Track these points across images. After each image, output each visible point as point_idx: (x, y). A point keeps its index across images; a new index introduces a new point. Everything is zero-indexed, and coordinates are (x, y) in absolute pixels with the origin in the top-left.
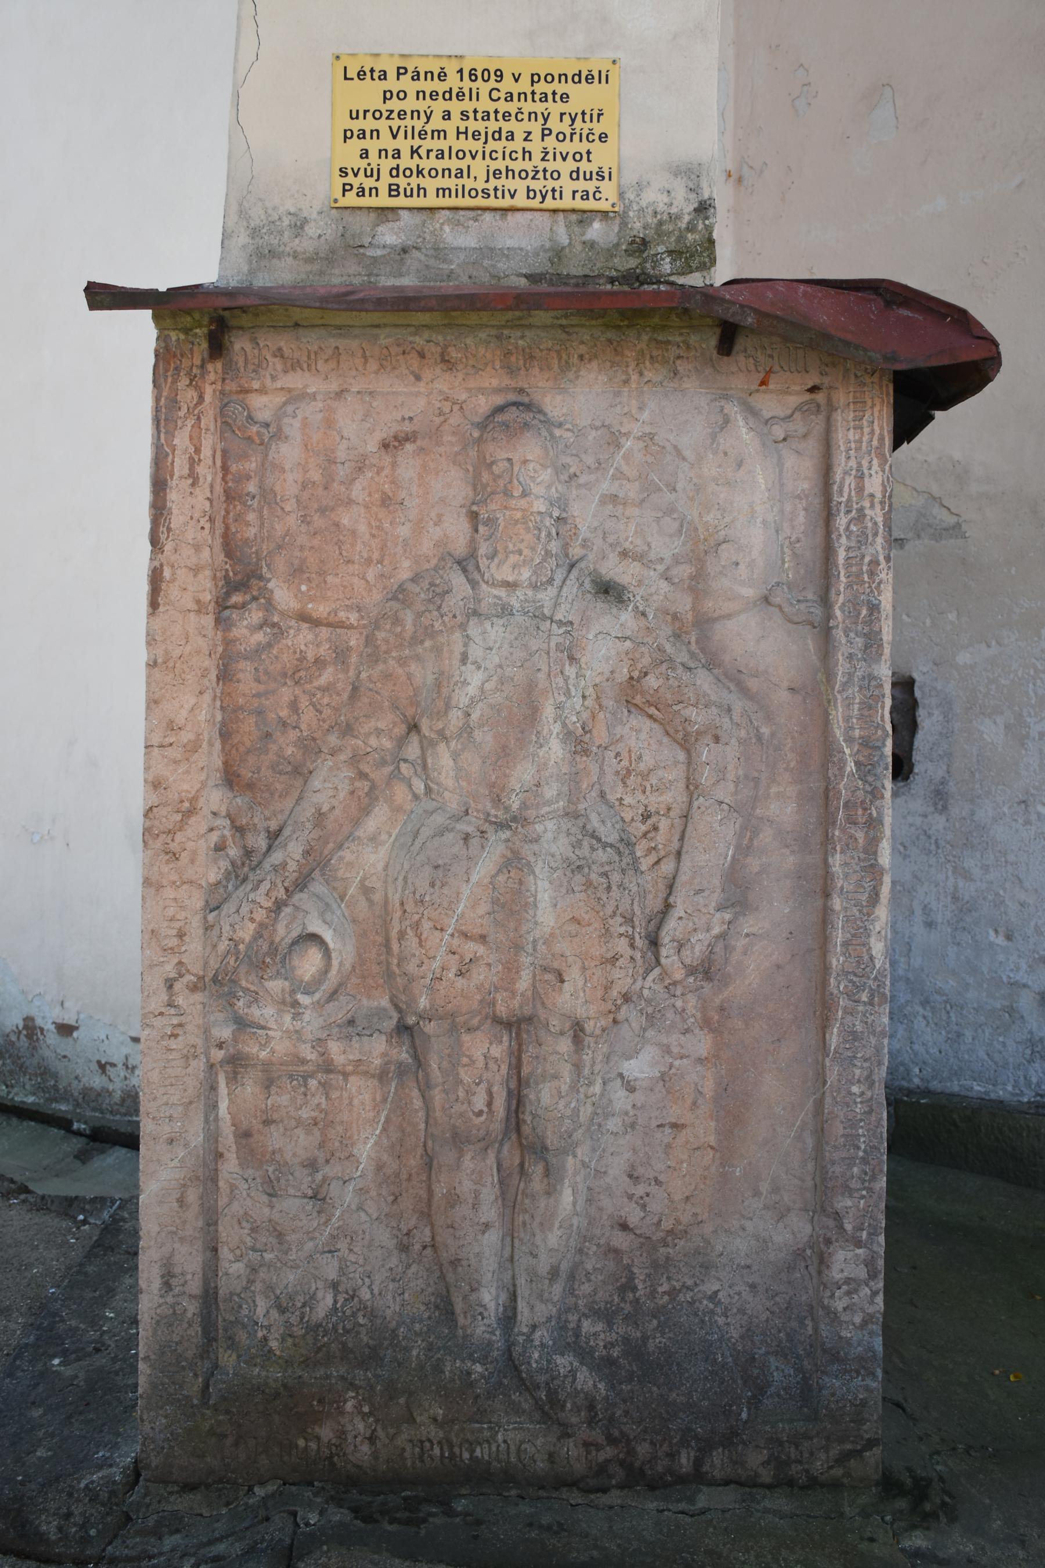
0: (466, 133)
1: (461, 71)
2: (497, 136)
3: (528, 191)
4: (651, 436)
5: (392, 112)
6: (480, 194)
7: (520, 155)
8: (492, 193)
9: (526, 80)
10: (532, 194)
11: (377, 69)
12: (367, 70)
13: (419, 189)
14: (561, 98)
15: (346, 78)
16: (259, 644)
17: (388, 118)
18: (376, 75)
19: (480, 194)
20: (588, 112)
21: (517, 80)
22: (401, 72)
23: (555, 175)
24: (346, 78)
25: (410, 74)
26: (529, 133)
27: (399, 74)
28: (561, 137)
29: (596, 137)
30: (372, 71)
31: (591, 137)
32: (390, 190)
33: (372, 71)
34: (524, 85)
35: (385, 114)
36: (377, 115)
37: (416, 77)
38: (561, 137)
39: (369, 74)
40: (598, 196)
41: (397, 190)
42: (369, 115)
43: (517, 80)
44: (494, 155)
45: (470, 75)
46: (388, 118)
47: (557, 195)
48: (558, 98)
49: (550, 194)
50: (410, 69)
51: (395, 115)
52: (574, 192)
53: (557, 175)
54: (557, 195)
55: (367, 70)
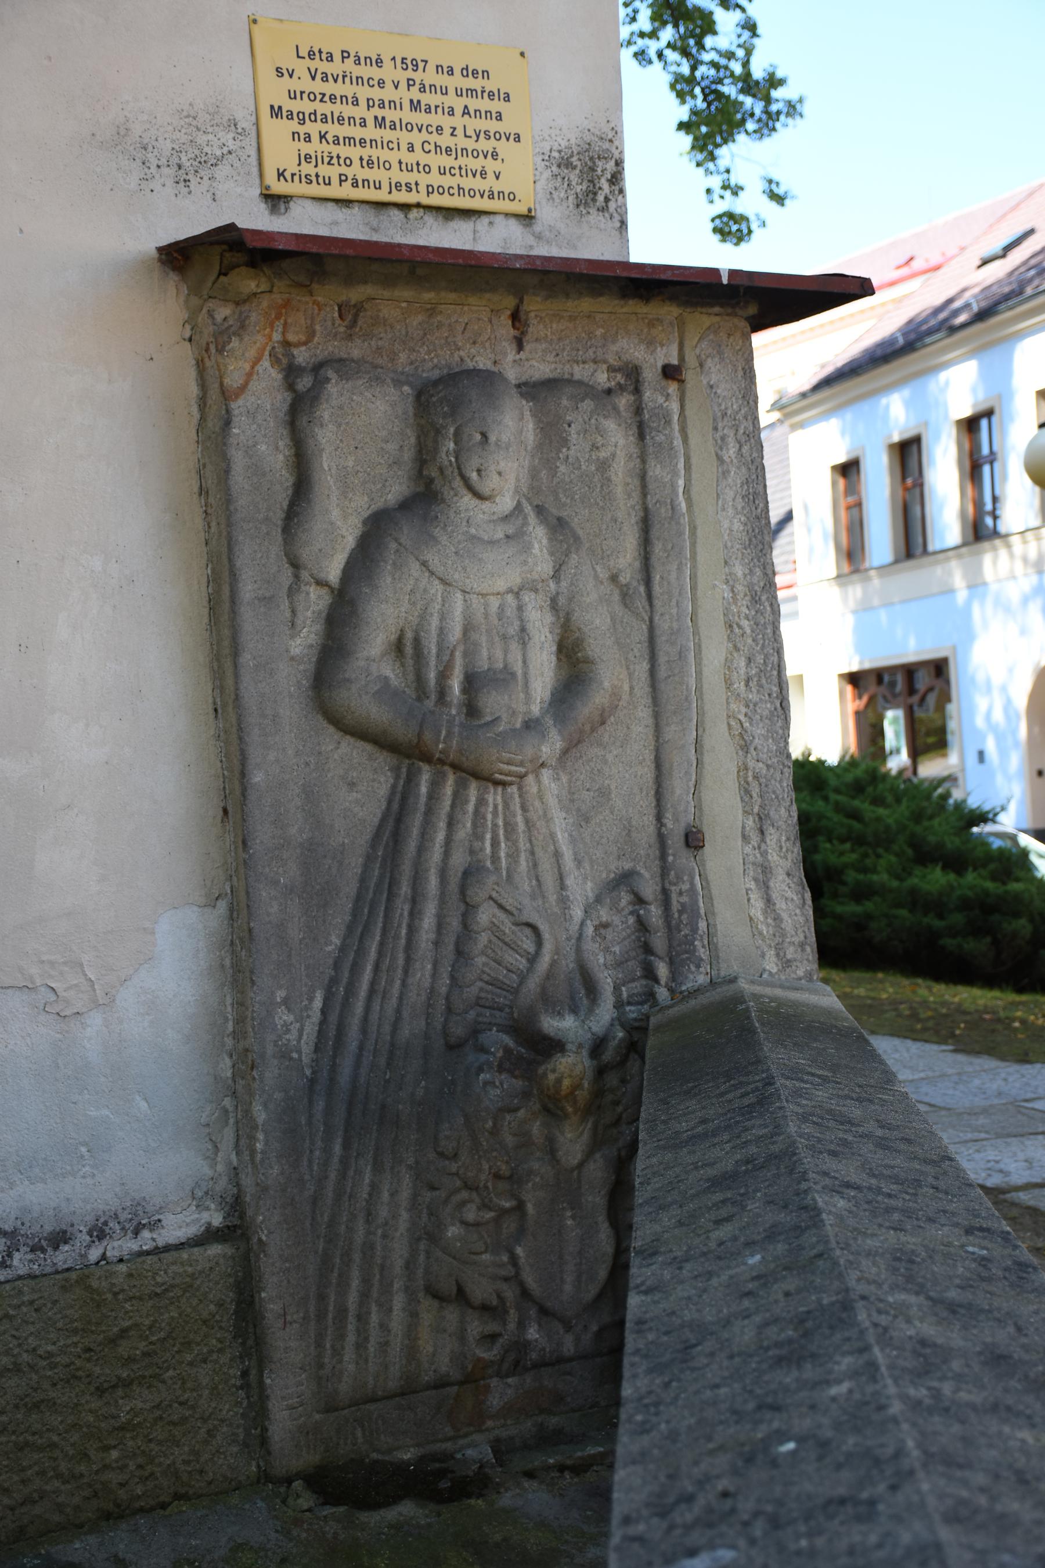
1: (394, 59)
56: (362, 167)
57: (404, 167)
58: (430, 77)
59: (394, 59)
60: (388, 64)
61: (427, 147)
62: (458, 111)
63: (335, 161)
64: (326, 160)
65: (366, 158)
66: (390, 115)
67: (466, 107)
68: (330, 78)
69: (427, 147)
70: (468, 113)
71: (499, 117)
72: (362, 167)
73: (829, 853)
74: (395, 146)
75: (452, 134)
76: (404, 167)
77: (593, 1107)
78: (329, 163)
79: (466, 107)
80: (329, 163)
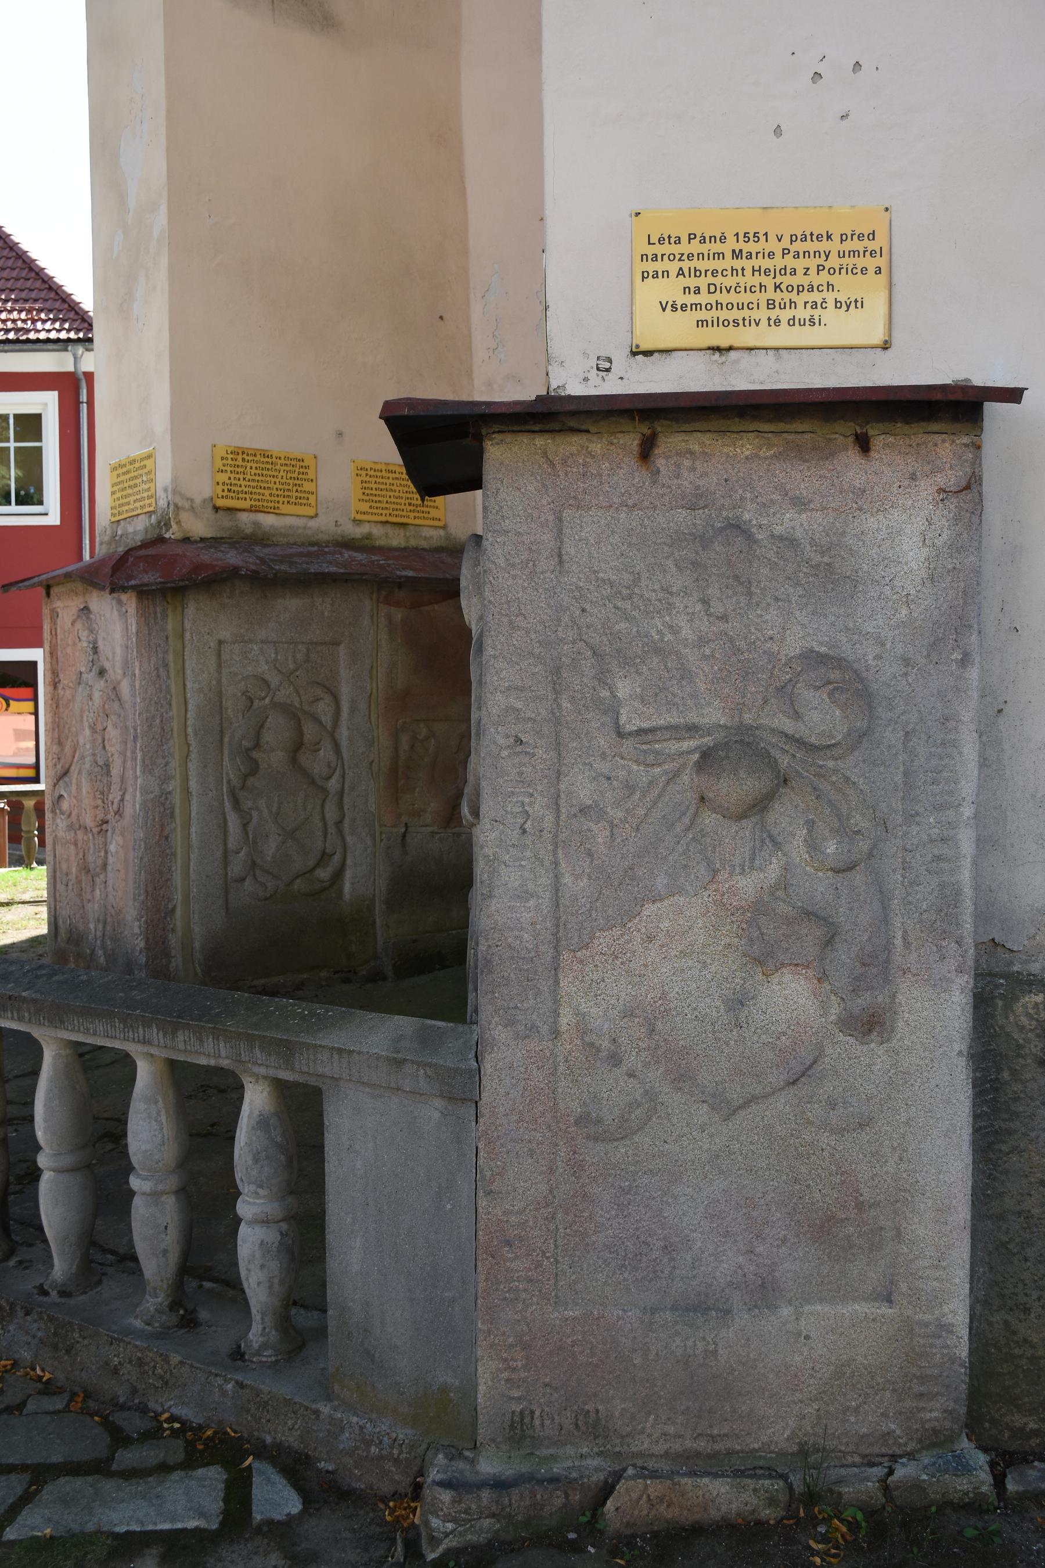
0: (759, 271)
1: (737, 234)
2: (783, 272)
3: (836, 302)
5: (683, 255)
6: (732, 323)
8: (741, 322)
9: (786, 240)
10: (839, 305)
11: (673, 236)
12: (666, 236)
13: (791, 303)
14: (817, 238)
17: (680, 260)
18: (672, 240)
19: (732, 323)
21: (780, 240)
22: (691, 237)
25: (698, 239)
26: (805, 274)
27: (690, 239)
28: (832, 271)
29: (859, 271)
30: (669, 237)
31: (855, 271)
32: (768, 304)
34: (786, 243)
35: (678, 257)
36: (672, 257)
37: (703, 240)
38: (832, 271)
39: (667, 240)
40: (824, 305)
42: (666, 258)
43: (780, 240)
46: (680, 260)
47: (859, 305)
48: (814, 238)
49: (853, 304)
51: (685, 257)
52: (806, 303)
53: (289, 484)
55: (666, 236)
59: (737, 234)
67: (681, 269)
70: (683, 274)
79: (681, 269)
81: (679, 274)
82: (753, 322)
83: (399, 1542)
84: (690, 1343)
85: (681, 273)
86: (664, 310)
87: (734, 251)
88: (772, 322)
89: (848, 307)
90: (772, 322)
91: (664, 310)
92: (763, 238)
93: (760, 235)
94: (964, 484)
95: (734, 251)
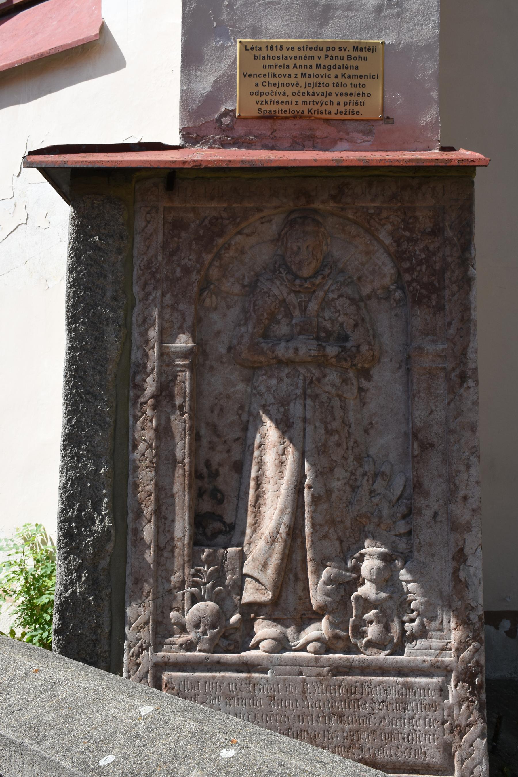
1: (267, 47)
2: (334, 67)
4: (473, 510)
7: (329, 103)
15: (246, 50)
16: (225, 117)
20: (305, 47)
21: (319, 59)
23: (364, 86)
24: (246, 50)
30: (256, 47)
32: (348, 58)
33: (256, 47)
39: (255, 49)
41: (351, 58)
44: (299, 94)
45: (271, 48)
47: (362, 104)
50: (330, 56)
54: (362, 104)
55: (254, 47)
56: (334, 87)
57: (353, 86)
58: (337, 53)
59: (267, 47)
60: (264, 49)
61: (264, 84)
62: (291, 66)
63: (321, 85)
64: (318, 85)
65: (336, 83)
66: (309, 71)
67: (295, 64)
68: (288, 58)
69: (264, 84)
70: (296, 67)
71: (357, 68)
72: (334, 87)
73: (231, 648)
74: (376, 77)
75: (295, 77)
76: (353, 86)
77: (390, 292)
78: (319, 86)
79: (295, 64)
80: (319, 86)
81: (294, 67)
82: (277, 94)
83: (157, 325)
84: (46, 634)
85: (295, 66)
86: (245, 76)
87: (317, 65)
88: (335, 85)
89: (322, 104)
90: (335, 85)
91: (245, 76)
92: (275, 49)
93: (274, 47)
94: (372, 553)
95: (317, 65)
